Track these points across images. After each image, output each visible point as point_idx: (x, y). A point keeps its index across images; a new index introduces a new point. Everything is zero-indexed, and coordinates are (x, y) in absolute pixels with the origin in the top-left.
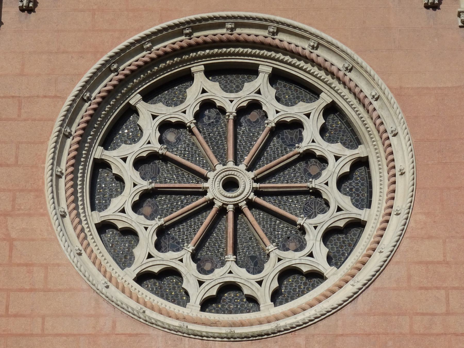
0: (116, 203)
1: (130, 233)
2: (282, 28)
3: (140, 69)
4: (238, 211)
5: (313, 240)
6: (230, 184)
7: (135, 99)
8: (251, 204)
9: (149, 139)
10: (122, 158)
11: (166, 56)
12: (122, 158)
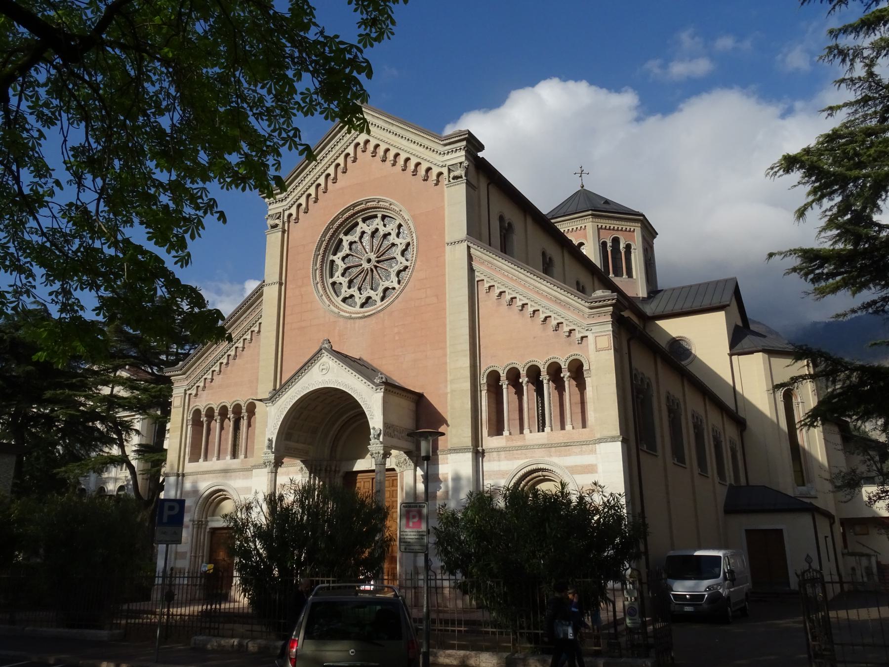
0: (343, 291)
1: (352, 296)
2: (368, 201)
3: (326, 249)
4: (376, 267)
5: (400, 258)
6: (369, 261)
7: (331, 257)
8: (378, 262)
9: (341, 265)
10: (338, 277)
11: (330, 239)
12: (338, 277)
